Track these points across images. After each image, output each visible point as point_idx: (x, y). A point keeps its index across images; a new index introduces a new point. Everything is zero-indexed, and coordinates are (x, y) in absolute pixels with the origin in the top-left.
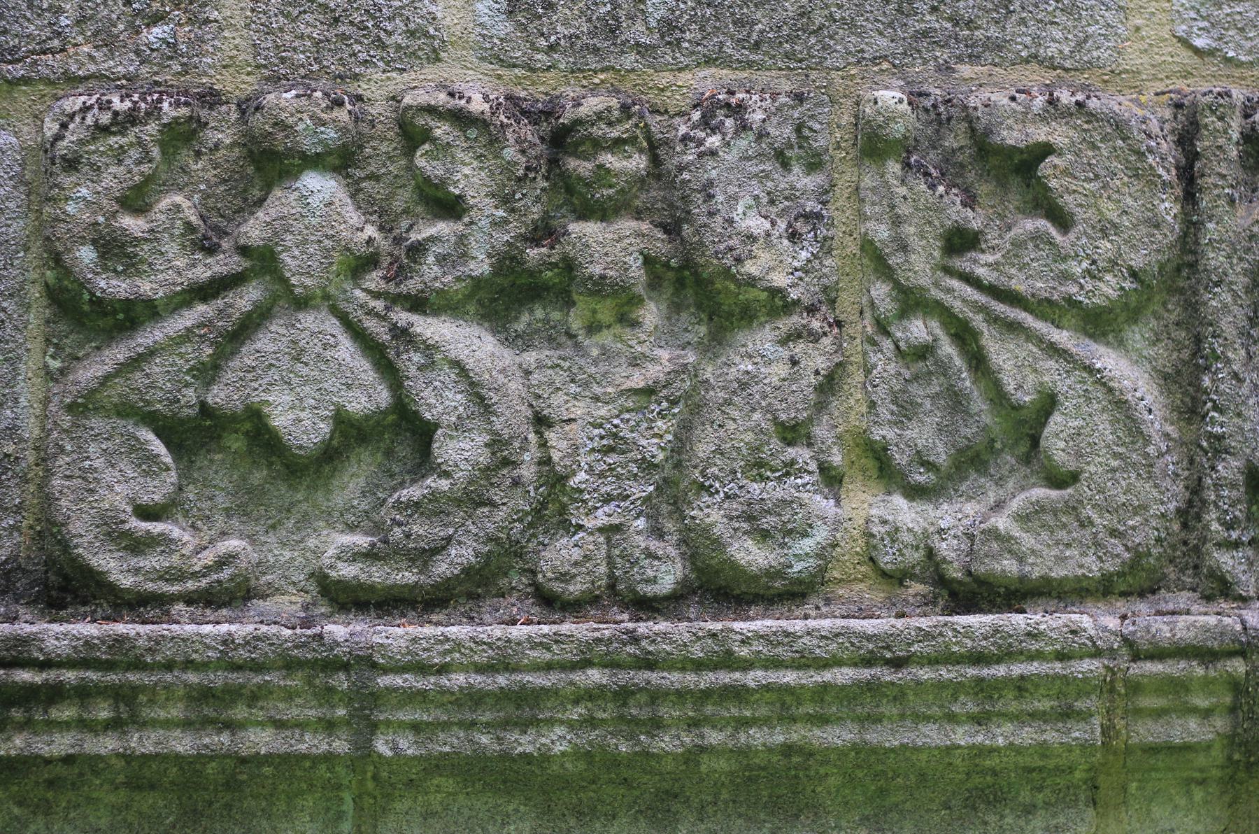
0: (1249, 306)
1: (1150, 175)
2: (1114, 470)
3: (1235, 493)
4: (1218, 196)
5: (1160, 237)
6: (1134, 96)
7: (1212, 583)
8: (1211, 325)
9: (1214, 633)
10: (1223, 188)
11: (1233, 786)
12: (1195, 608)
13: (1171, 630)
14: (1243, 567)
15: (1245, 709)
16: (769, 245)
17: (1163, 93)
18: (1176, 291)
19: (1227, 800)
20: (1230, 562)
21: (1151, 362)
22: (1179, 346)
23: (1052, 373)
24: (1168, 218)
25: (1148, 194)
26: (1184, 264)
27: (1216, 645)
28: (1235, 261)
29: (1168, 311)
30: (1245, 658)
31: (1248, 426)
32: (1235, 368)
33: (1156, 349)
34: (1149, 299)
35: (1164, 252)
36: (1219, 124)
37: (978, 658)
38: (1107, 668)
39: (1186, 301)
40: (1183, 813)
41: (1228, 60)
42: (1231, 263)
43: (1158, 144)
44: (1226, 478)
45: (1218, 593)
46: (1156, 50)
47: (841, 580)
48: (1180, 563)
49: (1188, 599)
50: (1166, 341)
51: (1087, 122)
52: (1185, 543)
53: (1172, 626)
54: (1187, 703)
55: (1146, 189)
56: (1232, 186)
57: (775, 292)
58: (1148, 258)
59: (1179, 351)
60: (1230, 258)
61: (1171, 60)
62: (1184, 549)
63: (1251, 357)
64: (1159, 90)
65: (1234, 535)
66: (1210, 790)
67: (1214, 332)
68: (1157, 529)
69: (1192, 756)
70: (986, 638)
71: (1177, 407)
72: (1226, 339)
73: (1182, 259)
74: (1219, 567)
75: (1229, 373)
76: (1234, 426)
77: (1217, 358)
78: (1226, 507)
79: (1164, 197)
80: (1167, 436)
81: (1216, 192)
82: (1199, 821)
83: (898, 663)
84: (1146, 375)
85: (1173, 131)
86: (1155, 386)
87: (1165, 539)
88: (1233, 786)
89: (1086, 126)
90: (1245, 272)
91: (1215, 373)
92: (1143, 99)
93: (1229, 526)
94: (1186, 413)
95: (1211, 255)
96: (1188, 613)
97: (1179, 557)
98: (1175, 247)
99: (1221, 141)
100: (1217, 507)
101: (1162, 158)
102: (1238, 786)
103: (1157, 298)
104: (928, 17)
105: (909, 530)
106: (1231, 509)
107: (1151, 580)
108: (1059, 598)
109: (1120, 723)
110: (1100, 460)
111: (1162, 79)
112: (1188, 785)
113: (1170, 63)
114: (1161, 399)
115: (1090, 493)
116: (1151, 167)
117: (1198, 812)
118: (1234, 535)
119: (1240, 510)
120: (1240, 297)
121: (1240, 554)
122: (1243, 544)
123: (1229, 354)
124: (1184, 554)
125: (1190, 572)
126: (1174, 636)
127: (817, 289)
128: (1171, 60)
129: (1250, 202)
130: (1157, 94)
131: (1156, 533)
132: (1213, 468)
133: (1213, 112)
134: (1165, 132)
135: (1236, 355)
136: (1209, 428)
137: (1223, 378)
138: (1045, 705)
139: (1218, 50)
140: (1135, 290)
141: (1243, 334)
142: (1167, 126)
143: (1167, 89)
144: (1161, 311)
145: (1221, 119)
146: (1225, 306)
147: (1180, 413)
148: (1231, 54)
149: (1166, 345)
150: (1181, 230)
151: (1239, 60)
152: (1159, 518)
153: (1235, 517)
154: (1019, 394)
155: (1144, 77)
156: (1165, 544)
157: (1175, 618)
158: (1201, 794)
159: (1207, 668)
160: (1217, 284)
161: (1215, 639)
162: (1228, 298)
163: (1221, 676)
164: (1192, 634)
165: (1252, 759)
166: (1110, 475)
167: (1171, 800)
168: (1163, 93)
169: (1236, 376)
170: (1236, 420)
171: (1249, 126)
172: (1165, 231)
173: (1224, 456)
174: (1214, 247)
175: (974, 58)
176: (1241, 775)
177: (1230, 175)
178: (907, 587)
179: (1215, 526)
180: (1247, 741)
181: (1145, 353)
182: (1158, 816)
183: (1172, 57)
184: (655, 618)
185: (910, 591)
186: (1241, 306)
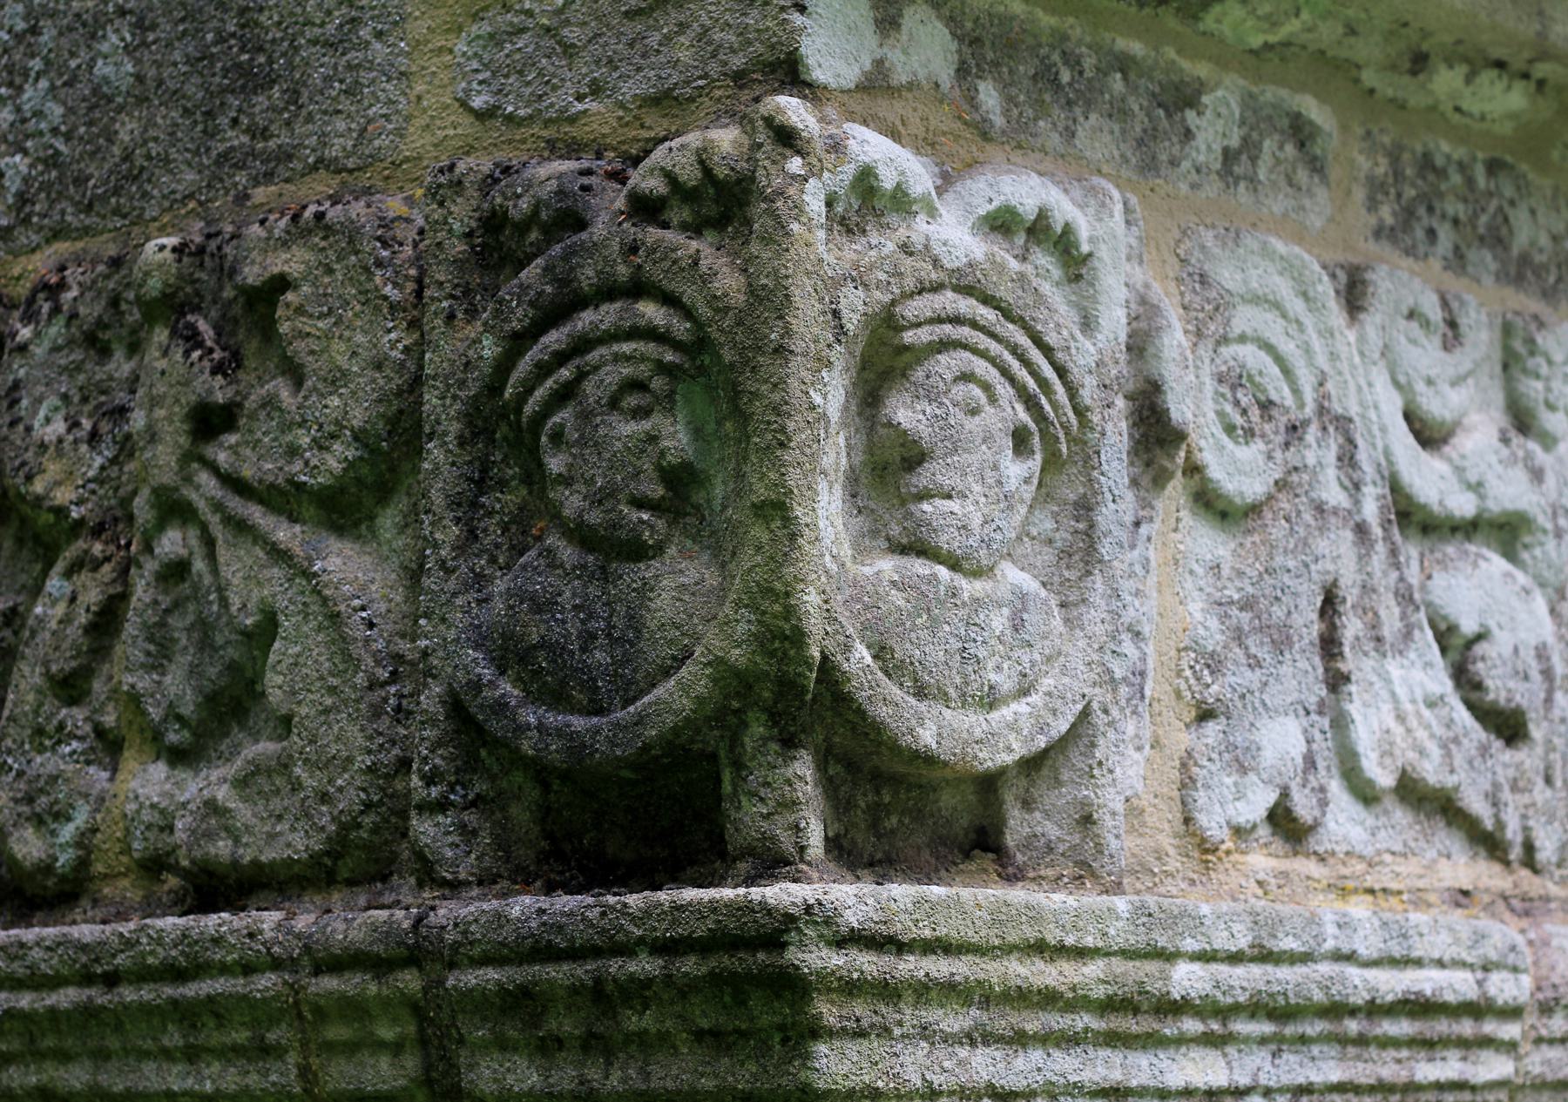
2: (327, 711)
14: (450, 839)
16: (60, 453)
20: (432, 831)
23: (275, 586)
28: (448, 402)
30: (421, 969)
32: (443, 553)
37: (176, 973)
38: (285, 983)
41: (510, 119)
47: (106, 876)
51: (325, 238)
56: (452, 297)
57: (61, 512)
61: (452, 132)
63: (476, 537)
70: (175, 946)
83: (112, 980)
89: (323, 244)
104: (230, 133)
105: (153, 806)
107: (377, 861)
108: (281, 891)
109: (315, 1062)
110: (311, 697)
115: (301, 743)
123: (438, 536)
127: (113, 502)
138: (241, 1036)
139: (499, 107)
140: (361, 458)
154: (242, 615)
166: (323, 718)
175: (269, 177)
178: (164, 882)
184: (1140, 993)
185: (166, 887)
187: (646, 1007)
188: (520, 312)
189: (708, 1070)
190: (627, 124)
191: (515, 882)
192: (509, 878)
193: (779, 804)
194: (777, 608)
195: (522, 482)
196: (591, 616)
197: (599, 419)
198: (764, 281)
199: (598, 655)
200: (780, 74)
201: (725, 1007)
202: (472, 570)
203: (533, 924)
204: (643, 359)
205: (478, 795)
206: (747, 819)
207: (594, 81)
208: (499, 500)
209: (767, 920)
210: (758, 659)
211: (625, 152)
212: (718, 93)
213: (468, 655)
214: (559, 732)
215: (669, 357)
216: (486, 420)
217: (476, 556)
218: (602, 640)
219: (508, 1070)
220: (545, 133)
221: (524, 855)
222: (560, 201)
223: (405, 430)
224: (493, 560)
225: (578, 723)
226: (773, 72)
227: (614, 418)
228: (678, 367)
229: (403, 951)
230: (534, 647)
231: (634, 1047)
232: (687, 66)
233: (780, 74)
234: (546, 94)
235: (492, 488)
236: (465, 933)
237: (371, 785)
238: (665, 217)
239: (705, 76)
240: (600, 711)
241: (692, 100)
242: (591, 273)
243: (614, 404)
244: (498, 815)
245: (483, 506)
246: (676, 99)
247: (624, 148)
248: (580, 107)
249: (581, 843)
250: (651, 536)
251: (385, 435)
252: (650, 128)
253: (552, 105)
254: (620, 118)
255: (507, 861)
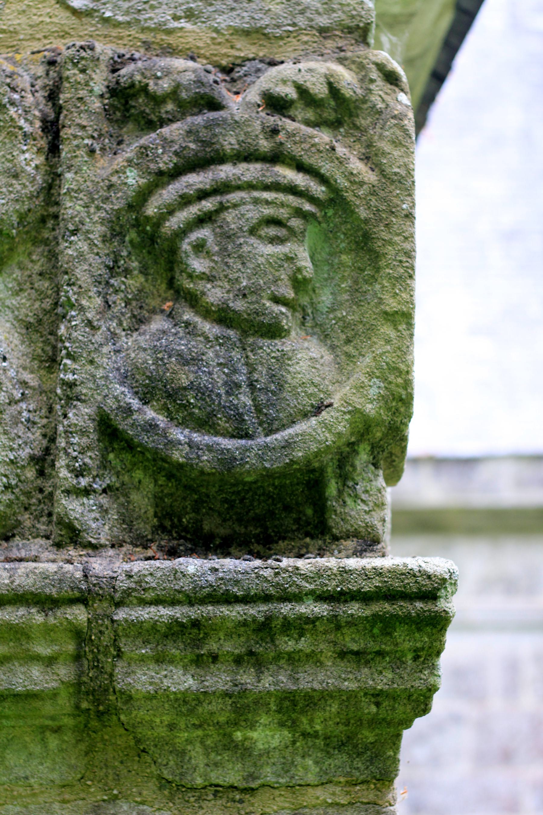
0: (107, 255)
1: (11, 126)
3: (85, 441)
4: (78, 146)
5: (19, 188)
6: (10, 55)
7: (61, 530)
8: (66, 273)
9: (53, 580)
10: (83, 139)
11: (88, 734)
12: (45, 555)
13: (10, 577)
14: (93, 515)
15: (90, 657)
17: (39, 52)
18: (41, 242)
19: (83, 748)
20: (79, 509)
21: (13, 312)
22: (42, 295)
24: (28, 169)
25: (8, 146)
26: (48, 216)
27: (54, 592)
28: (92, 210)
29: (32, 261)
30: (86, 605)
31: (100, 373)
33: (19, 298)
34: (11, 250)
35: (23, 202)
36: (81, 77)
39: (50, 251)
40: (38, 760)
41: (106, 21)
42: (88, 212)
43: (22, 97)
44: (76, 425)
45: (68, 541)
46: (35, 11)
48: (35, 510)
49: (41, 546)
50: (29, 291)
52: (41, 491)
53: (11, 573)
54: (29, 650)
55: (7, 141)
56: (93, 137)
58: (5, 208)
59: (41, 301)
60: (87, 207)
61: (48, 20)
62: (40, 496)
63: (109, 306)
64: (35, 50)
65: (84, 482)
66: (66, 738)
67: (70, 279)
68: (6, 476)
69: (38, 704)
71: (39, 356)
72: (80, 287)
73: (46, 211)
74: (66, 514)
75: (83, 321)
76: (86, 373)
77: (72, 306)
78: (75, 454)
79: (25, 148)
80: (24, 384)
81: (75, 143)
82: (53, 770)
84: (8, 325)
85: (44, 87)
86: (16, 335)
87: (17, 486)
88: (88, 734)
90: (103, 222)
91: (70, 321)
92: (18, 57)
93: (79, 473)
94: (46, 361)
95: (69, 204)
96: (35, 559)
97: (34, 505)
98: (37, 197)
99: (82, 93)
100: (67, 454)
101: (25, 111)
102: (93, 735)
103: (21, 249)
106: (81, 456)
111: (39, 39)
112: (43, 732)
113: (47, 24)
114: (22, 348)
116: (12, 119)
117: (54, 760)
118: (84, 482)
119: (90, 457)
120: (96, 246)
121: (92, 502)
122: (95, 491)
123: (84, 302)
124: (40, 501)
125: (44, 519)
126: (12, 582)
128: (48, 20)
129: (115, 154)
130: (33, 53)
131: (5, 480)
132: (65, 416)
133: (75, 65)
134: (37, 87)
135: (91, 302)
136: (62, 376)
137: (76, 325)
139: (96, 11)
141: (100, 283)
142: (39, 83)
143: (44, 49)
144: (26, 261)
145: (83, 71)
146: (81, 254)
147: (41, 361)
148: (108, 14)
149: (29, 294)
150: (45, 181)
151: (116, 20)
152: (8, 464)
153: (84, 464)
155: (22, 37)
156: (17, 491)
157: (17, 564)
158: (56, 742)
159: (46, 615)
160: (74, 233)
161: (53, 586)
162: (84, 247)
163: (61, 624)
164: (30, 581)
165: (101, 708)
167: (26, 747)
168: (39, 52)
169: (89, 323)
170: (89, 367)
171: (114, 80)
172: (24, 181)
173: (75, 403)
174: (71, 197)
176: (94, 723)
177: (91, 126)
179: (64, 473)
180: (94, 690)
181: (8, 302)
182: (12, 764)
183: (50, 17)
186: (97, 254)
187: (301, 635)
188: (166, 158)
189: (351, 676)
190: (219, 44)
191: (137, 546)
192: (131, 543)
193: (375, 504)
194: (400, 380)
195: (141, 272)
196: (235, 371)
197: (242, 240)
198: (397, 170)
199: (242, 398)
200: (356, 35)
201: (373, 636)
202: (109, 330)
203: (210, 578)
204: (282, 205)
205: (108, 485)
206: (353, 513)
207: (190, 10)
208: (124, 283)
209: (427, 582)
210: (382, 412)
211: (216, 61)
212: (305, 38)
213: (116, 389)
214: (210, 448)
215: (307, 207)
216: (121, 226)
217: (110, 319)
218: (244, 388)
219: (166, 676)
220: (142, 36)
221: (145, 529)
222: (199, 87)
223: (29, 223)
224: (120, 324)
225: (226, 443)
226: (350, 33)
227: (252, 240)
228: (313, 215)
229: (77, 594)
230: (185, 389)
231: (282, 662)
232: (278, 16)
233: (356, 35)
234: (144, 10)
235: (118, 274)
236: (139, 583)
237: (12, 473)
238: (291, 113)
239: (294, 25)
240: (247, 436)
241: (281, 38)
242: (233, 141)
243: (253, 231)
244: (122, 499)
245: (112, 286)
246: (264, 34)
247: (215, 59)
248: (176, 24)
249: (180, 521)
250: (287, 324)
251: (16, 225)
252: (239, 50)
253: (151, 19)
254: (213, 39)
255: (130, 531)
